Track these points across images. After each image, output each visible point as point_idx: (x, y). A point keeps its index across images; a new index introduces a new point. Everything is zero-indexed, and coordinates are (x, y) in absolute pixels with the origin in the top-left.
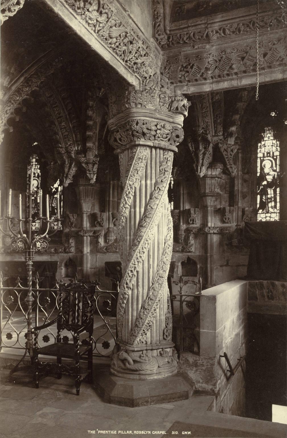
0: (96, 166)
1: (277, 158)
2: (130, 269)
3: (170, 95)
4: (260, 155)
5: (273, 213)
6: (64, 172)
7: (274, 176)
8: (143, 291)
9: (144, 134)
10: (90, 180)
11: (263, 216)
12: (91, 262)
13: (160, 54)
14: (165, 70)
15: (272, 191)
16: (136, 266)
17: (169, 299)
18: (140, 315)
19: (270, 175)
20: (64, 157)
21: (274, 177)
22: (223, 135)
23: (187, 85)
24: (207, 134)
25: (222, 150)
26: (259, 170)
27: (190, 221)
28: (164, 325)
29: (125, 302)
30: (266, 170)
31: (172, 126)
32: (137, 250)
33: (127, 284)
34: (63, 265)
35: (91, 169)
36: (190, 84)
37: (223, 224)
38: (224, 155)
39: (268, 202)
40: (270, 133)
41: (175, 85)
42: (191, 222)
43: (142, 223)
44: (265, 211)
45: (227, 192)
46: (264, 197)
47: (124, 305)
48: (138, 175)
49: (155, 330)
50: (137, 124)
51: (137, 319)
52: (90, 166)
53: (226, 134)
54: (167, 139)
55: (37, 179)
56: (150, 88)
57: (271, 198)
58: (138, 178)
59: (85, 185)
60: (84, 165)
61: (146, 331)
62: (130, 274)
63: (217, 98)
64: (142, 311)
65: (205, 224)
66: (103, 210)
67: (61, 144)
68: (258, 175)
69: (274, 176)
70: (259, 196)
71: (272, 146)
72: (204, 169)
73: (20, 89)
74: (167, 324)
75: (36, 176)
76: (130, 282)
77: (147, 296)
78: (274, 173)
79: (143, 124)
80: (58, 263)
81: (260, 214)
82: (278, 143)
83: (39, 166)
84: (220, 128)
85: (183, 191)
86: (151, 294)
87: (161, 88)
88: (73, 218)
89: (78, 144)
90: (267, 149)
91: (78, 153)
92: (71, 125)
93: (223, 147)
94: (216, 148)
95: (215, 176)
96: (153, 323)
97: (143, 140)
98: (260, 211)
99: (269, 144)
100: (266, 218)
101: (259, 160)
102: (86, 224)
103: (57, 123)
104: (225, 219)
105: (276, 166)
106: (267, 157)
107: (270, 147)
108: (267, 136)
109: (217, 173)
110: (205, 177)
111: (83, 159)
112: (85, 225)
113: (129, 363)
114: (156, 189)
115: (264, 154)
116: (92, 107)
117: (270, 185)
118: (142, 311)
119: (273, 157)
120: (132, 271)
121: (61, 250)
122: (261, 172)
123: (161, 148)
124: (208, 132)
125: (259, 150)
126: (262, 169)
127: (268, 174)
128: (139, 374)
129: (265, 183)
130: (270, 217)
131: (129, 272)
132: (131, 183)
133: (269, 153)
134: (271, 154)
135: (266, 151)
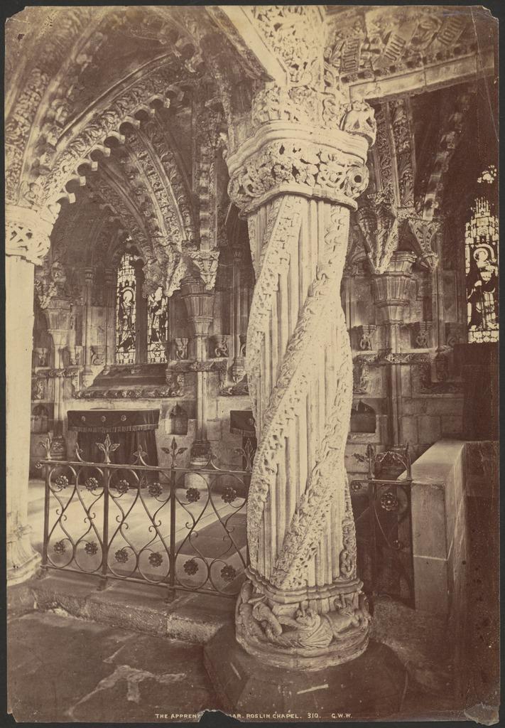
0: (215, 264)
1: (497, 244)
2: (273, 434)
3: (343, 102)
4: (469, 241)
5: (494, 330)
6: (167, 275)
7: (494, 272)
8: (299, 475)
9: (295, 171)
10: (205, 285)
11: (478, 335)
12: (214, 409)
13: (322, 20)
14: (333, 53)
15: (491, 295)
16: (284, 427)
17: (348, 489)
18: (292, 525)
19: (487, 271)
20: (167, 252)
21: (493, 274)
22: (415, 206)
23: (374, 81)
24: (390, 205)
25: (414, 230)
26: (468, 265)
27: (363, 344)
28: (340, 546)
29: (264, 497)
30: (480, 264)
31: (375, 104)
32: (286, 397)
33: (266, 462)
34: (168, 415)
35: (207, 268)
36: (380, 78)
37: (415, 348)
38: (418, 239)
39: (486, 314)
40: (484, 207)
41: (352, 83)
42: (364, 348)
43: (293, 342)
44: (481, 327)
45: (418, 299)
46: (478, 305)
47: (262, 503)
48: (285, 250)
49: (323, 557)
50: (282, 150)
51: (287, 534)
52: (207, 264)
53: (419, 205)
54: (340, 182)
55: (130, 289)
56: (306, 87)
57: (489, 308)
58: (284, 257)
59: (199, 294)
60: (196, 262)
61: (305, 559)
62: (273, 443)
63: (404, 147)
64: (298, 517)
65: (386, 350)
66: (225, 332)
67: (161, 232)
68: (468, 271)
69: (494, 272)
70: (470, 305)
71: (488, 226)
72: (386, 261)
73: (87, 132)
74: (348, 542)
75: (130, 285)
76: (272, 458)
77: (307, 488)
78: (493, 267)
79: (294, 151)
80: (161, 413)
81: (473, 332)
82: (497, 221)
83: (133, 270)
84: (410, 195)
85: (350, 299)
86: (314, 483)
87: (325, 88)
88: (181, 345)
89: (188, 231)
90: (480, 231)
91: (186, 245)
92: (176, 203)
93: (415, 225)
94: (405, 226)
95: (401, 273)
96: (320, 543)
97: (293, 182)
98: (473, 328)
99: (483, 224)
100: (482, 338)
101: (467, 249)
102: (202, 353)
103: (154, 199)
104: (419, 340)
105: (496, 257)
106: (481, 243)
107: (486, 228)
108: (480, 211)
109: (404, 270)
110: (386, 274)
111: (194, 254)
112: (199, 355)
113: (274, 631)
114: (320, 277)
115: (475, 239)
116: (207, 171)
117: (486, 287)
118: (298, 517)
119: (490, 244)
120: (275, 437)
121: (164, 393)
122: (471, 267)
123: (327, 201)
124: (391, 200)
125: (467, 233)
126: (473, 262)
127: (484, 270)
128: (296, 656)
129: (479, 283)
130: (490, 337)
131: (271, 439)
132: (271, 266)
133: (485, 237)
134: (488, 238)
135: (479, 234)
